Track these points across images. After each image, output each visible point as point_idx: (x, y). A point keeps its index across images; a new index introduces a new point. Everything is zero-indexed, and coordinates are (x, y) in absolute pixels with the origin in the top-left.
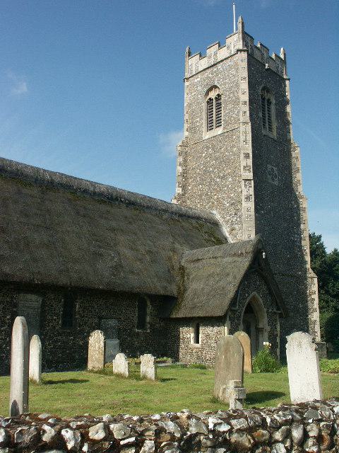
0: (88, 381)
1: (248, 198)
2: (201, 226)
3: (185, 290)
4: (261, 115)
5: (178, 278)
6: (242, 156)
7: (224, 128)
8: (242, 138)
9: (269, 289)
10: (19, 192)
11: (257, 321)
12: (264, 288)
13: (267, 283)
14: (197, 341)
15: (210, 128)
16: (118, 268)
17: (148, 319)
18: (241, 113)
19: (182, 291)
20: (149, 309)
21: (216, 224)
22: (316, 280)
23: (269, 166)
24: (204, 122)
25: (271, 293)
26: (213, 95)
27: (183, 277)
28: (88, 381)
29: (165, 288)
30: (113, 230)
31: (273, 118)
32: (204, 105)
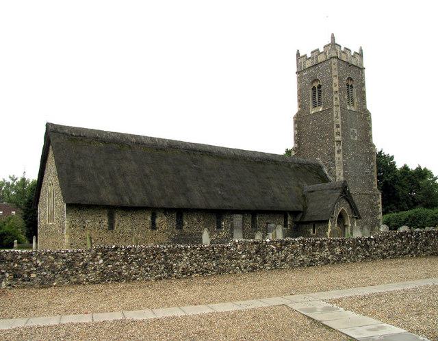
0: (333, 34)
1: (338, 152)
2: (311, 169)
3: (307, 208)
4: (346, 97)
5: (302, 201)
6: (335, 126)
7: (324, 107)
8: (335, 115)
9: (350, 205)
10: (222, 164)
11: (344, 222)
12: (348, 205)
13: (349, 202)
14: (314, 232)
15: (314, 106)
16: (274, 198)
17: (289, 222)
18: (333, 85)
19: (305, 208)
20: (289, 218)
21: (320, 167)
22: (380, 196)
23: (352, 129)
24: (311, 102)
25: (351, 207)
26: (316, 85)
27: (305, 200)
28: (333, 34)
29: (296, 207)
30: (268, 178)
31: (355, 96)
32: (311, 92)
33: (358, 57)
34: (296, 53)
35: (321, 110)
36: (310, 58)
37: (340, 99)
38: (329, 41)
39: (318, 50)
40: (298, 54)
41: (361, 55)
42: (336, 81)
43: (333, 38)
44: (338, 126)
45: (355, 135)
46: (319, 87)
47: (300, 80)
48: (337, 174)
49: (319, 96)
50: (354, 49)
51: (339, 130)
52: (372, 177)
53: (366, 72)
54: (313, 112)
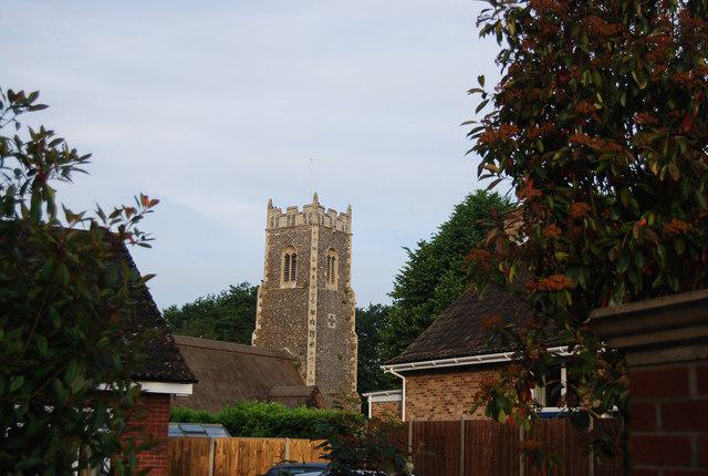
0: (154, 276)
23: (334, 327)
28: (154, 276)
33: (345, 220)
34: (43, 103)
35: (294, 286)
36: (284, 215)
37: (318, 277)
38: (310, 201)
39: (295, 208)
40: (270, 206)
41: (349, 217)
42: (314, 254)
43: (316, 197)
44: (313, 313)
45: (332, 322)
46: (294, 256)
47: (272, 240)
48: (308, 373)
49: (294, 267)
50: (341, 209)
51: (315, 317)
52: (351, 376)
53: (353, 238)
54: (283, 287)
